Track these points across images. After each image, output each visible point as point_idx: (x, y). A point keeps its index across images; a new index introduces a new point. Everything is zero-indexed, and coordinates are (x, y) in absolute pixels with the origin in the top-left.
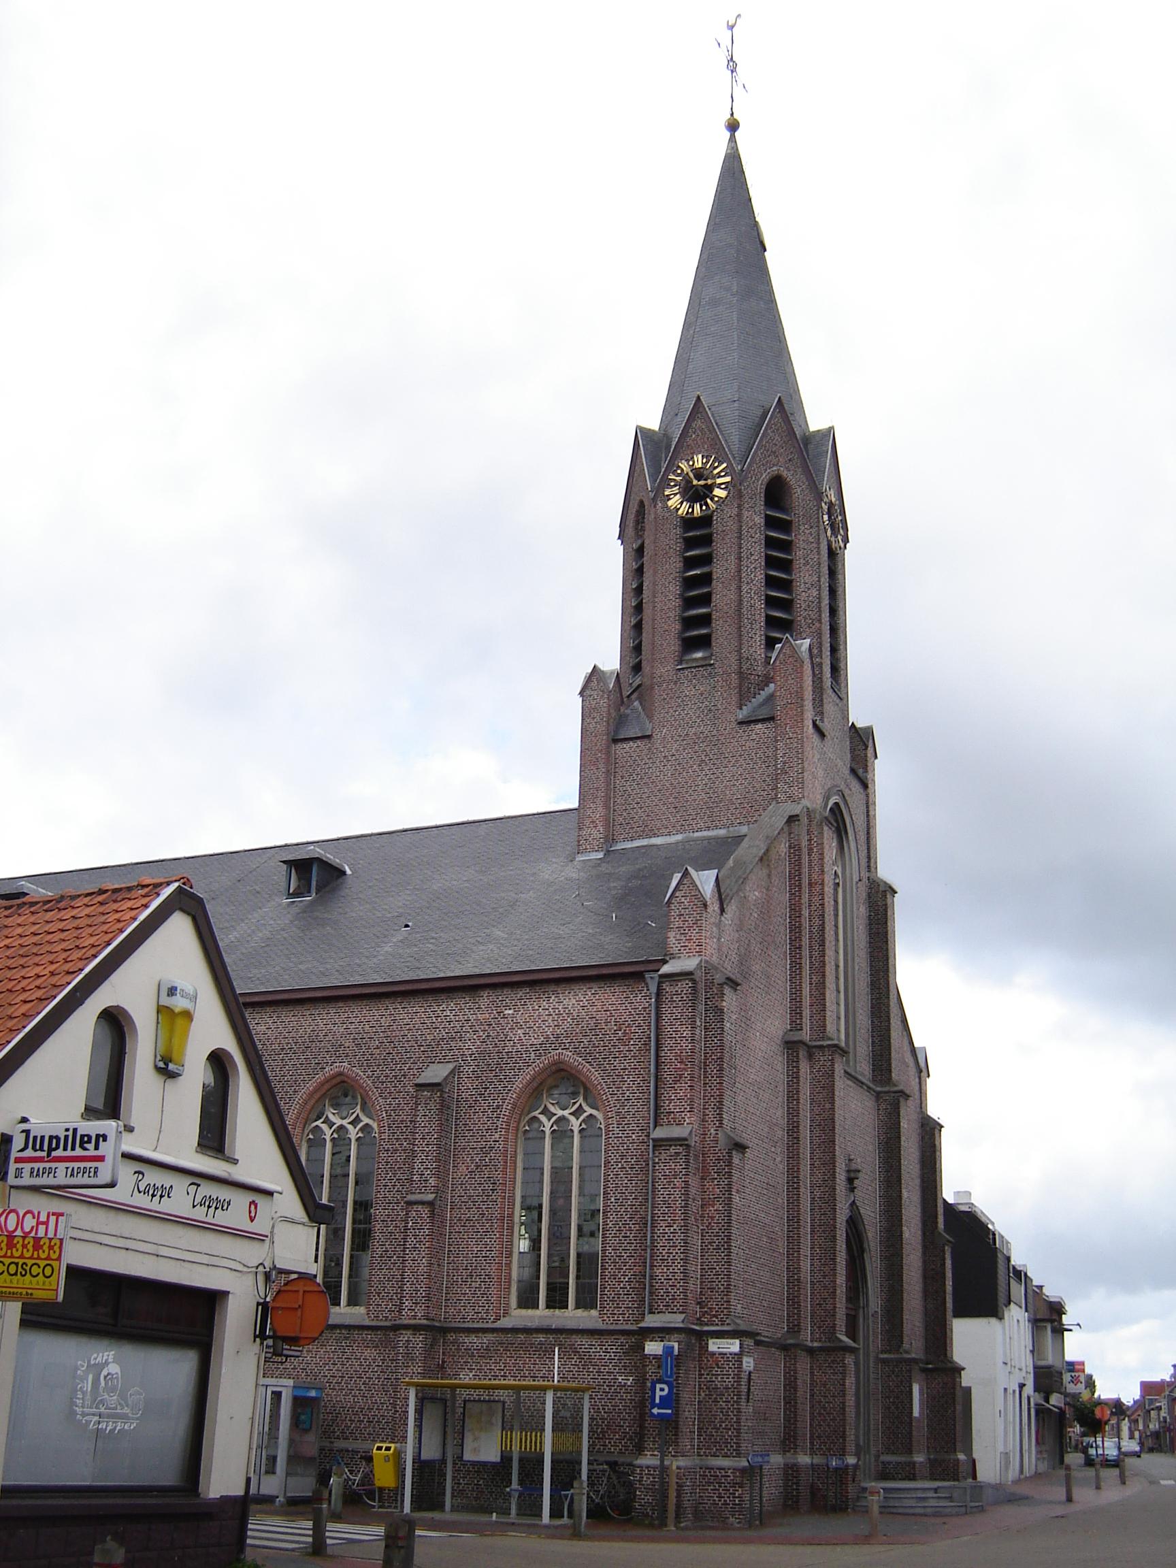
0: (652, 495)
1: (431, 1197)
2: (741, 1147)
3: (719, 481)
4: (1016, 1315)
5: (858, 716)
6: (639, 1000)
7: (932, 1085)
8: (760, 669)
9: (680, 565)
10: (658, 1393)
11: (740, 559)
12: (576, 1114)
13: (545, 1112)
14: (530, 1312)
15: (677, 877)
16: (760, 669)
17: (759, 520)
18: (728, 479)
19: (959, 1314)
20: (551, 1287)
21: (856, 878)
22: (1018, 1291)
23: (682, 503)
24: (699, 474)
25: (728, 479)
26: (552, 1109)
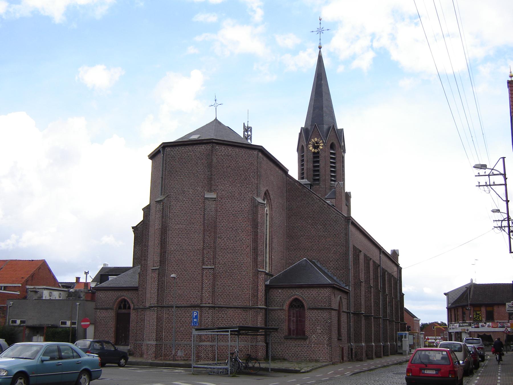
2: (361, 251)
24: (317, 143)
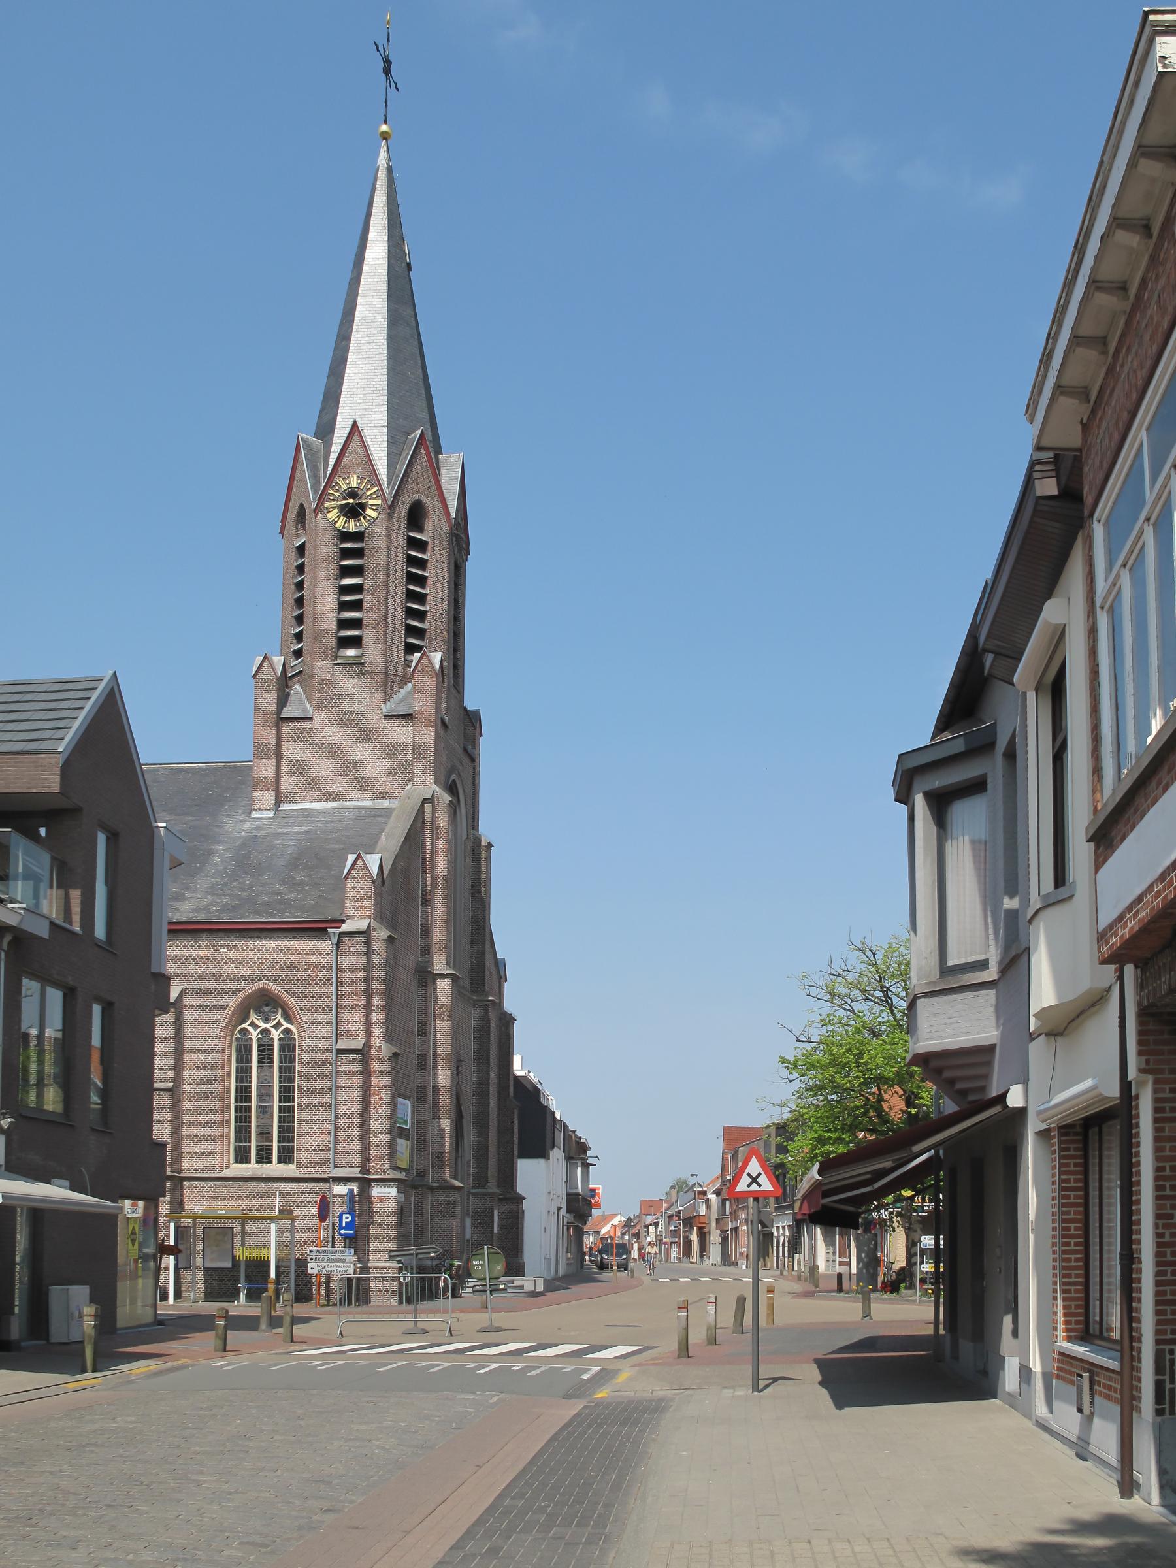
0: (314, 506)
1: (170, 1085)
3: (371, 502)
4: (557, 1154)
5: (470, 703)
6: (324, 947)
7: (507, 987)
8: (400, 671)
9: (336, 572)
10: (344, 1220)
11: (387, 575)
12: (276, 1026)
13: (252, 1024)
14: (244, 1165)
15: (351, 858)
16: (400, 671)
17: (403, 541)
18: (378, 502)
19: (523, 1155)
20: (259, 1149)
21: (464, 837)
22: (559, 1137)
23: (339, 517)
24: (352, 493)
25: (378, 502)
26: (257, 1022)
